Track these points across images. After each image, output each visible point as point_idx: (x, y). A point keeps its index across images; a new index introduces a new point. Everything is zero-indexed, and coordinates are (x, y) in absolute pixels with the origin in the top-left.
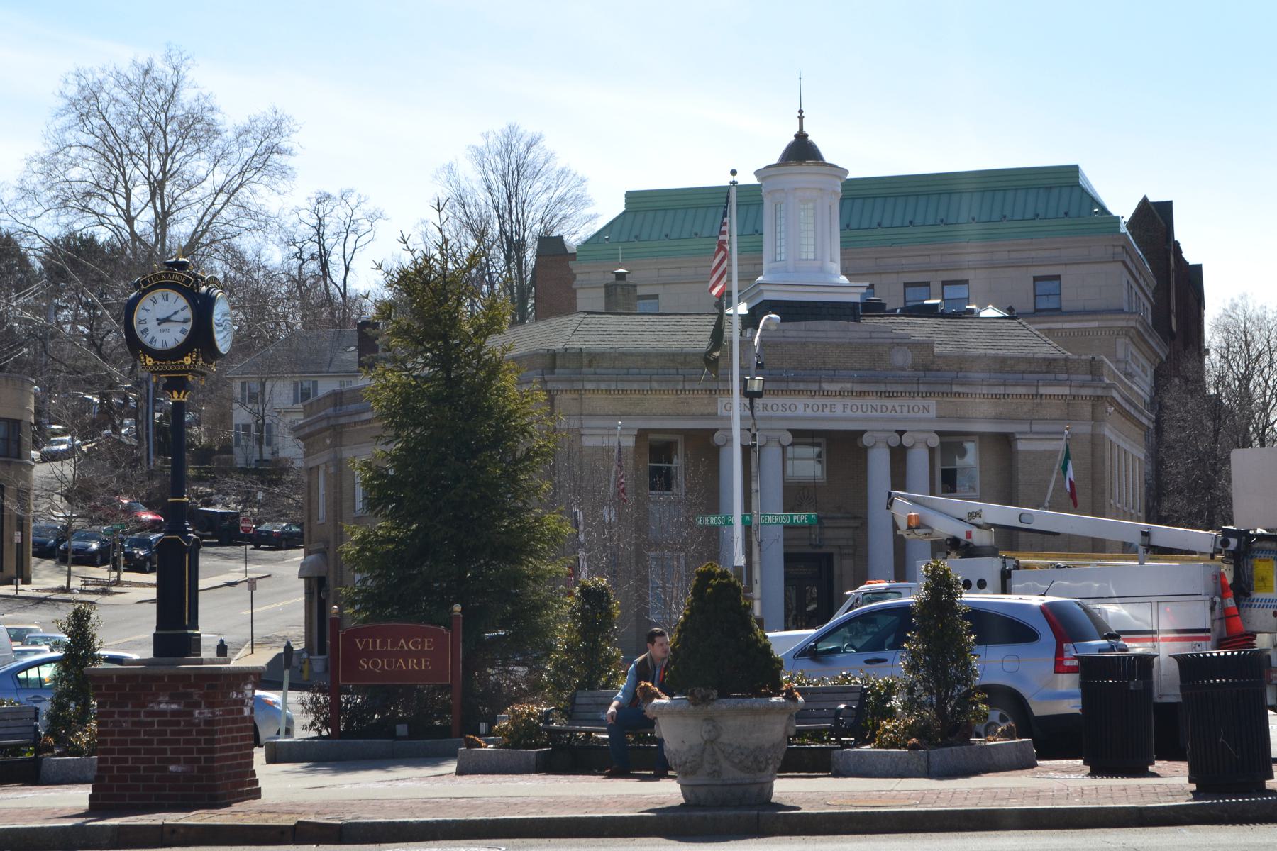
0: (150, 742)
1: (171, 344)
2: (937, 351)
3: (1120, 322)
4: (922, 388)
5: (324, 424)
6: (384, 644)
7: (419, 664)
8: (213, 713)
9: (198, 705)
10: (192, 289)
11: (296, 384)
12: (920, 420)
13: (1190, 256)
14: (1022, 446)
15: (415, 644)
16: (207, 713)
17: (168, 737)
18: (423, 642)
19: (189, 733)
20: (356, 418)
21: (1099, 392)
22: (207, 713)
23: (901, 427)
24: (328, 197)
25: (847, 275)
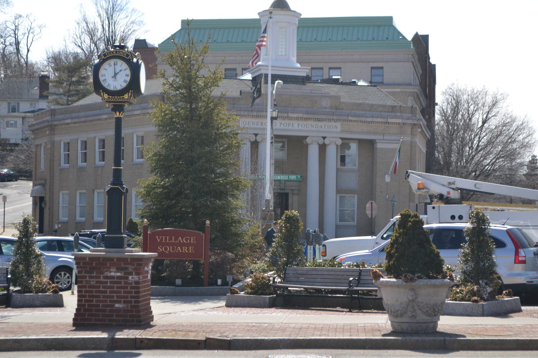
0: (105, 292)
1: (119, 88)
2: (342, 100)
3: (410, 89)
4: (335, 117)
5: (46, 124)
6: (170, 239)
7: (188, 250)
8: (139, 278)
9: (131, 274)
10: (129, 59)
11: (9, 103)
13: (432, 61)
14: (379, 146)
15: (186, 240)
16: (136, 278)
17: (115, 289)
18: (190, 239)
19: (127, 288)
20: (62, 122)
21: (415, 122)
22: (136, 278)
24: (21, 16)
25: (300, 63)
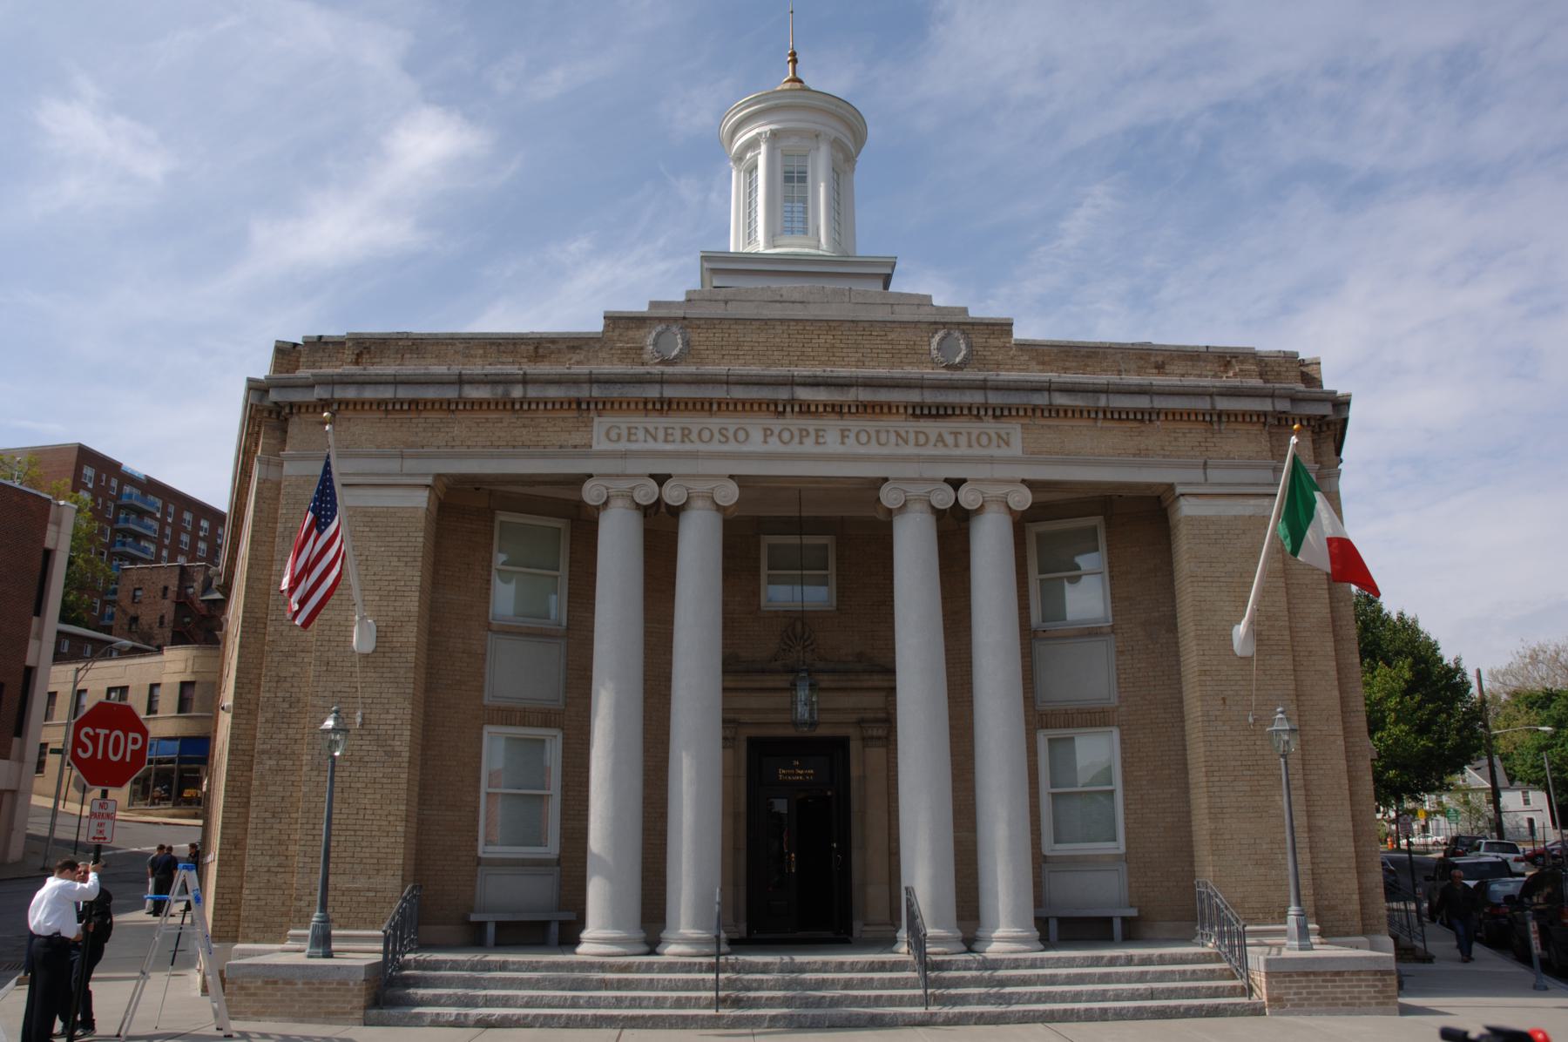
12: (991, 460)
14: (1187, 509)
23: (956, 472)
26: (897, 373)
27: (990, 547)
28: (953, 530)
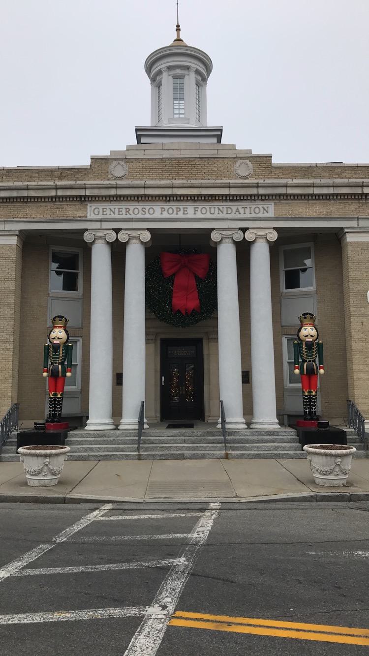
12: (260, 219)
14: (350, 238)
26: (219, 181)
27: (260, 257)
28: (243, 251)
